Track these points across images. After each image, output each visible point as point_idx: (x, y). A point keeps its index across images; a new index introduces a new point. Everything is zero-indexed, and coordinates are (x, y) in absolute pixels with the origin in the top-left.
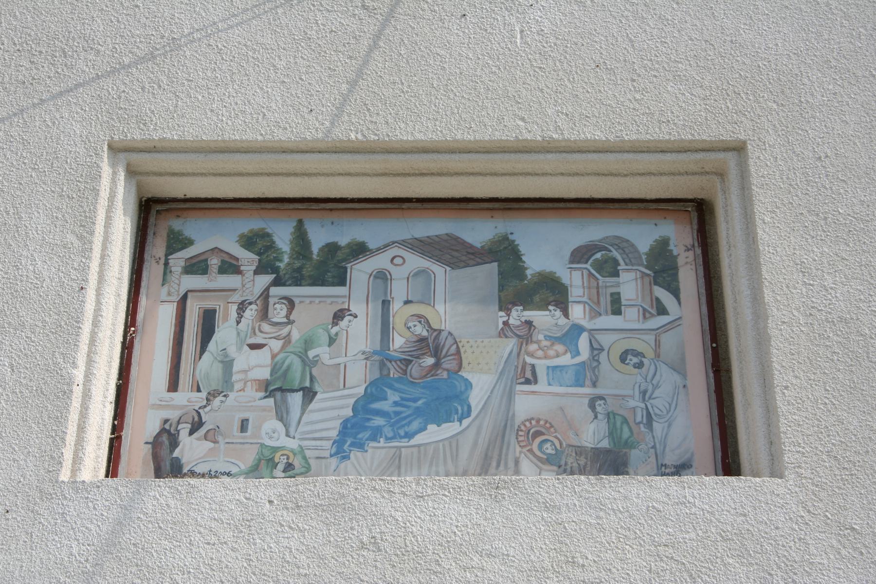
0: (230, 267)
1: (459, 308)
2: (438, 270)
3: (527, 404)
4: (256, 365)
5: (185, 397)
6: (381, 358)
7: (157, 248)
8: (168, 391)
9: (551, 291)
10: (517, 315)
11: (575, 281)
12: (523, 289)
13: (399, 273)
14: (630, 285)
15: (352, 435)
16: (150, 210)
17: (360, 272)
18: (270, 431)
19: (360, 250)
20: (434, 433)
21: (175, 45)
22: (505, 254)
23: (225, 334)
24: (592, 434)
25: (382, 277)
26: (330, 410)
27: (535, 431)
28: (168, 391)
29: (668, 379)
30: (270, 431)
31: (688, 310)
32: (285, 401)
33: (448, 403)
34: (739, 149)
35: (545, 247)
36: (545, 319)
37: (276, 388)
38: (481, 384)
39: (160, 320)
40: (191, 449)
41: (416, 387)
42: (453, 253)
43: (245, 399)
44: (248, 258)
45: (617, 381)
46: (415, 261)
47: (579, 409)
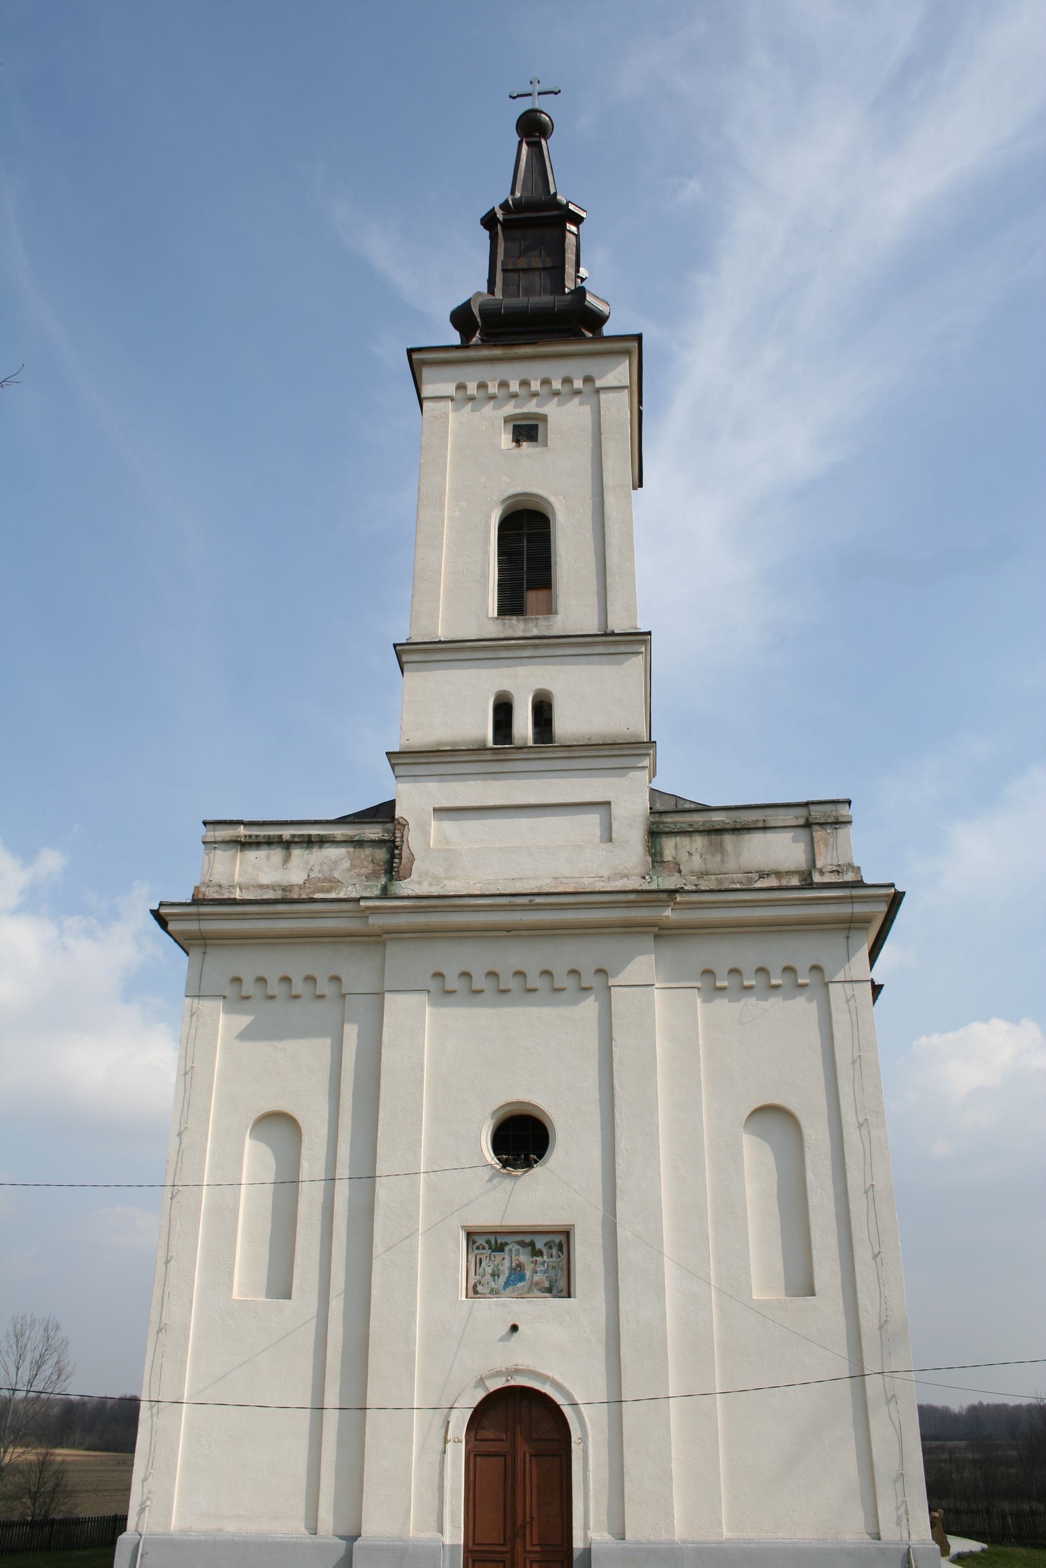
0: (484, 1248)
1: (524, 1258)
2: (521, 1248)
3: (536, 1278)
4: (489, 1270)
5: (478, 1277)
6: (511, 1268)
7: (471, 1244)
8: (936, 1426)
9: (540, 1253)
10: (535, 1258)
11: (545, 1251)
12: (536, 1253)
13: (514, 1250)
14: (554, 1251)
15: (507, 1284)
16: (469, 1235)
17: (507, 1248)
18: (493, 1285)
19: (506, 1244)
20: (520, 1284)
21: (471, 1202)
22: (532, 1244)
23: (484, 1263)
24: (547, 1284)
25: (510, 1250)
26: (503, 1279)
27: (537, 1284)
28: (936, 1426)
29: (560, 1272)
30: (493, 1285)
31: (564, 1256)
32: (864, 1381)
33: (522, 1278)
34: (573, 1225)
35: (539, 1245)
36: (539, 1259)
37: (493, 1275)
38: (528, 1273)
39: (472, 1259)
40: (479, 1288)
41: (517, 1273)
42: (522, 1244)
43: (488, 1277)
44: (487, 1246)
45: (552, 1273)
46: (517, 1247)
47: (544, 1279)
